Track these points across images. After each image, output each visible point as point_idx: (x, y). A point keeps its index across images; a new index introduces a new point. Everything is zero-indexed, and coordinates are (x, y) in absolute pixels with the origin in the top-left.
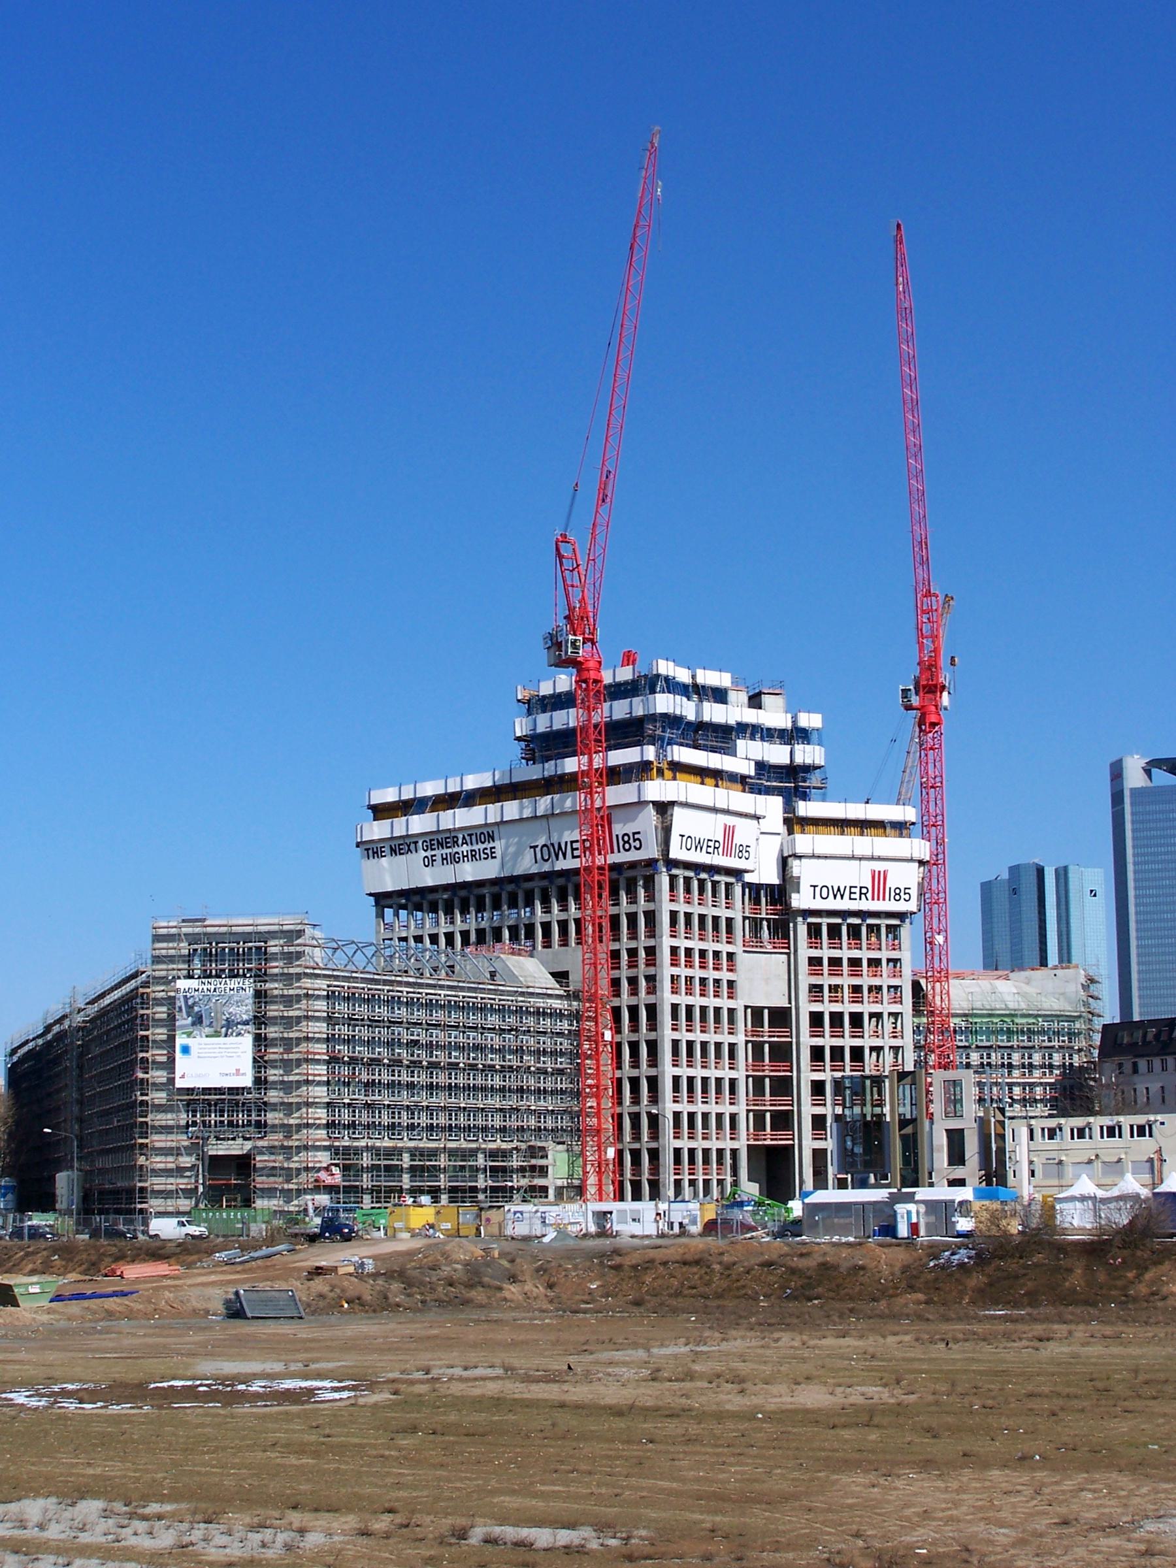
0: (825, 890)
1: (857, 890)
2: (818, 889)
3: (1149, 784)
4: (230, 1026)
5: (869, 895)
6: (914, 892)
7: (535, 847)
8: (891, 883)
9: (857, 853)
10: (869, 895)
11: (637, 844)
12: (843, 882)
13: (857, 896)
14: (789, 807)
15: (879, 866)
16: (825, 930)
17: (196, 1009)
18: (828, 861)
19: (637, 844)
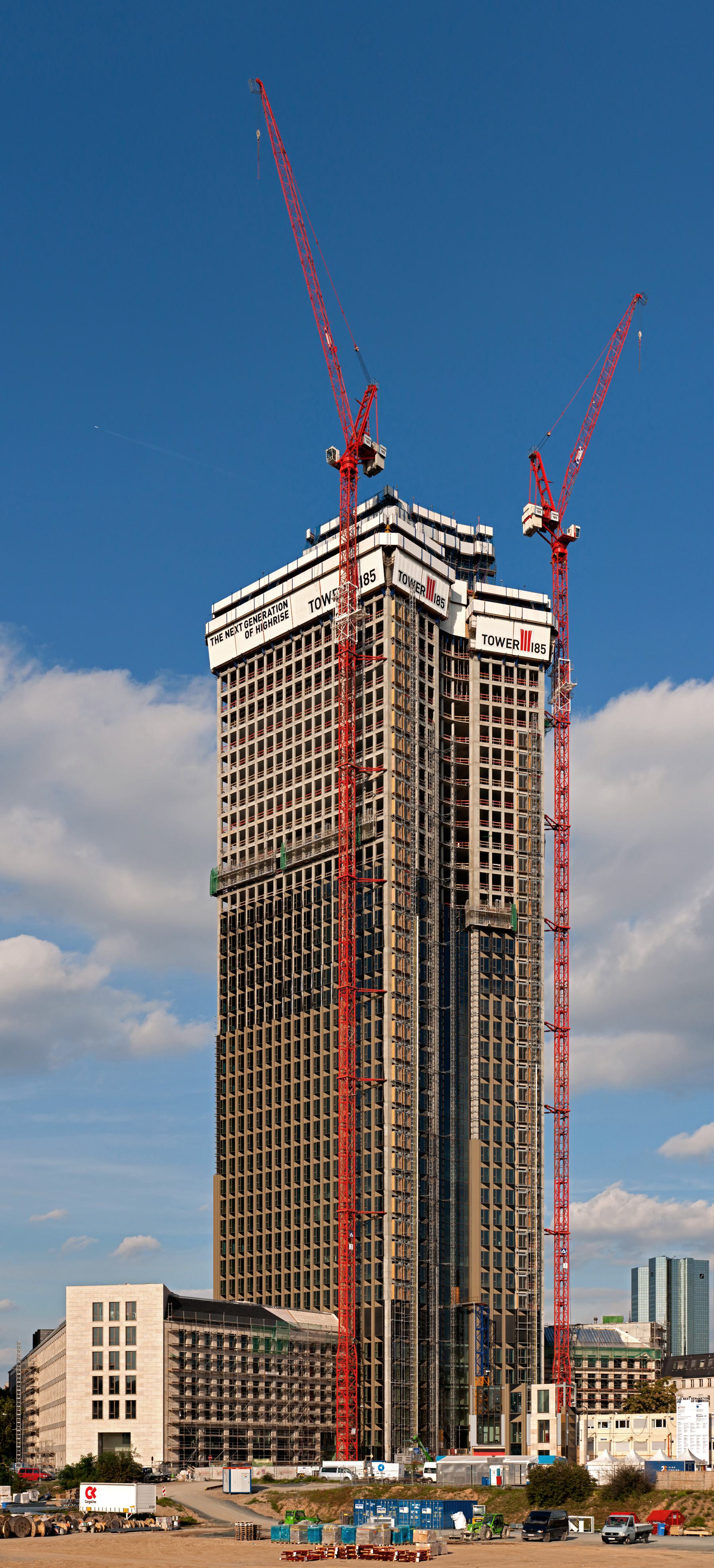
0: (491, 639)
1: (512, 642)
2: (487, 638)
3: (222, 1299)
4: (699, 1522)
5: (519, 646)
6: (547, 648)
7: (485, 636)
8: (534, 640)
9: (512, 616)
10: (519, 646)
11: (373, 578)
12: (503, 635)
13: (511, 646)
14: (470, 586)
15: (527, 627)
18: (497, 620)
19: (373, 578)
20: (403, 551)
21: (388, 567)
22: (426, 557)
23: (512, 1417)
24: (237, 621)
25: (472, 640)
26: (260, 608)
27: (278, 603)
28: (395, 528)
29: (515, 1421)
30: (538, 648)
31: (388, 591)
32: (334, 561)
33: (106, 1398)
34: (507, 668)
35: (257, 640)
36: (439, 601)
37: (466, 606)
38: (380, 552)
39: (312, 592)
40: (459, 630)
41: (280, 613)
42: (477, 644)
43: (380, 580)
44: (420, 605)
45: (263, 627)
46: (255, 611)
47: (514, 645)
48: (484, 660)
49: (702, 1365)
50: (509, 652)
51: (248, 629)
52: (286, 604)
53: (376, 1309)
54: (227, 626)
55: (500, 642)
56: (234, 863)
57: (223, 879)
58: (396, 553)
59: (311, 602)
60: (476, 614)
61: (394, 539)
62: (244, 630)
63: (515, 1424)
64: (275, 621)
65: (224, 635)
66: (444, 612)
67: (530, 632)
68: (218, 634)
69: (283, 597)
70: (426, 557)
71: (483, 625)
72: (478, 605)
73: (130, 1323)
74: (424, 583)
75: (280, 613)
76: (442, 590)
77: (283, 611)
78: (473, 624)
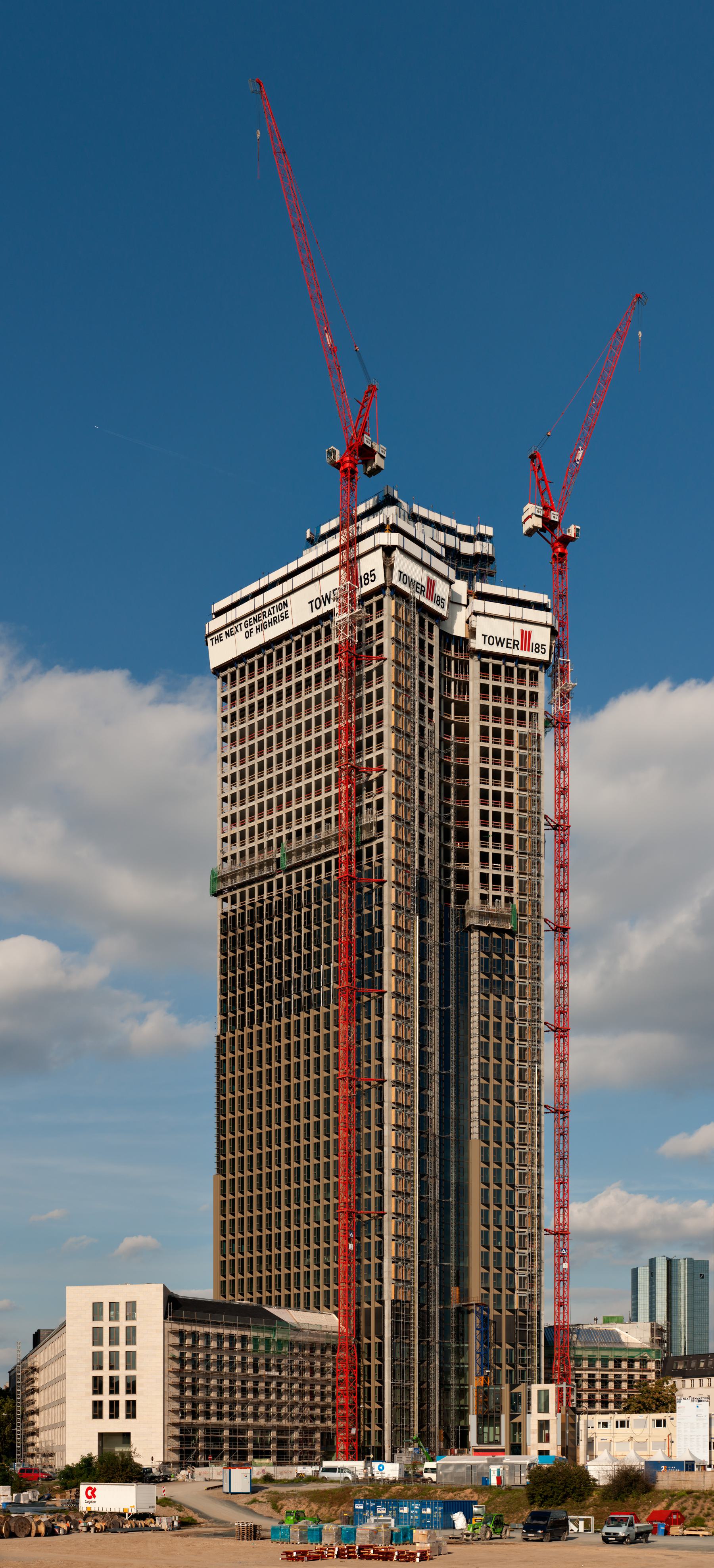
0: (491, 639)
1: (512, 642)
2: (487, 638)
5: (519, 646)
6: (547, 648)
7: (485, 636)
8: (534, 640)
9: (512, 616)
10: (519, 646)
12: (503, 635)
13: (511, 646)
15: (527, 627)
16: (528, 673)
17: (176, 1524)
18: (497, 620)
20: (403, 551)
21: (388, 567)
22: (426, 557)
23: (512, 1417)
24: (237, 621)
25: (472, 640)
26: (261, 608)
27: (278, 603)
28: (395, 528)
29: (515, 1421)
30: (538, 648)
31: (388, 591)
32: (334, 561)
33: (106, 1398)
34: (507, 668)
35: (257, 640)
36: (439, 601)
37: (466, 606)
38: (380, 552)
39: (313, 592)
40: (459, 630)
41: (280, 613)
42: (477, 644)
43: (380, 580)
44: (420, 605)
45: (263, 627)
46: (255, 611)
47: (514, 645)
48: (484, 660)
49: (702, 1365)
50: (509, 652)
51: (248, 629)
52: (286, 604)
53: (376, 1309)
54: (227, 626)
55: (500, 642)
56: (234, 862)
57: (223, 879)
58: (396, 553)
59: (311, 602)
60: (476, 614)
61: (394, 539)
62: (244, 630)
63: (515, 1424)
64: (275, 621)
65: (224, 635)
66: (444, 612)
67: (530, 632)
68: (218, 634)
69: (283, 597)
70: (426, 557)
71: (483, 626)
72: (478, 605)
73: (130, 1323)
74: (424, 583)
75: (280, 613)
76: (442, 589)
77: (283, 611)
78: (473, 624)
